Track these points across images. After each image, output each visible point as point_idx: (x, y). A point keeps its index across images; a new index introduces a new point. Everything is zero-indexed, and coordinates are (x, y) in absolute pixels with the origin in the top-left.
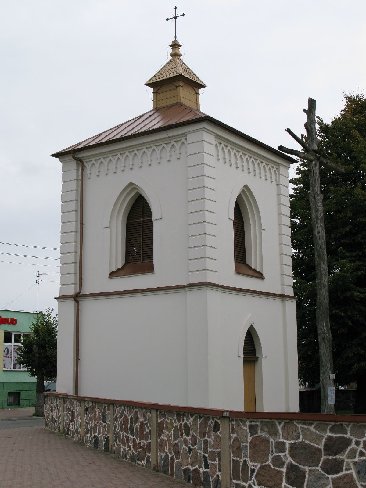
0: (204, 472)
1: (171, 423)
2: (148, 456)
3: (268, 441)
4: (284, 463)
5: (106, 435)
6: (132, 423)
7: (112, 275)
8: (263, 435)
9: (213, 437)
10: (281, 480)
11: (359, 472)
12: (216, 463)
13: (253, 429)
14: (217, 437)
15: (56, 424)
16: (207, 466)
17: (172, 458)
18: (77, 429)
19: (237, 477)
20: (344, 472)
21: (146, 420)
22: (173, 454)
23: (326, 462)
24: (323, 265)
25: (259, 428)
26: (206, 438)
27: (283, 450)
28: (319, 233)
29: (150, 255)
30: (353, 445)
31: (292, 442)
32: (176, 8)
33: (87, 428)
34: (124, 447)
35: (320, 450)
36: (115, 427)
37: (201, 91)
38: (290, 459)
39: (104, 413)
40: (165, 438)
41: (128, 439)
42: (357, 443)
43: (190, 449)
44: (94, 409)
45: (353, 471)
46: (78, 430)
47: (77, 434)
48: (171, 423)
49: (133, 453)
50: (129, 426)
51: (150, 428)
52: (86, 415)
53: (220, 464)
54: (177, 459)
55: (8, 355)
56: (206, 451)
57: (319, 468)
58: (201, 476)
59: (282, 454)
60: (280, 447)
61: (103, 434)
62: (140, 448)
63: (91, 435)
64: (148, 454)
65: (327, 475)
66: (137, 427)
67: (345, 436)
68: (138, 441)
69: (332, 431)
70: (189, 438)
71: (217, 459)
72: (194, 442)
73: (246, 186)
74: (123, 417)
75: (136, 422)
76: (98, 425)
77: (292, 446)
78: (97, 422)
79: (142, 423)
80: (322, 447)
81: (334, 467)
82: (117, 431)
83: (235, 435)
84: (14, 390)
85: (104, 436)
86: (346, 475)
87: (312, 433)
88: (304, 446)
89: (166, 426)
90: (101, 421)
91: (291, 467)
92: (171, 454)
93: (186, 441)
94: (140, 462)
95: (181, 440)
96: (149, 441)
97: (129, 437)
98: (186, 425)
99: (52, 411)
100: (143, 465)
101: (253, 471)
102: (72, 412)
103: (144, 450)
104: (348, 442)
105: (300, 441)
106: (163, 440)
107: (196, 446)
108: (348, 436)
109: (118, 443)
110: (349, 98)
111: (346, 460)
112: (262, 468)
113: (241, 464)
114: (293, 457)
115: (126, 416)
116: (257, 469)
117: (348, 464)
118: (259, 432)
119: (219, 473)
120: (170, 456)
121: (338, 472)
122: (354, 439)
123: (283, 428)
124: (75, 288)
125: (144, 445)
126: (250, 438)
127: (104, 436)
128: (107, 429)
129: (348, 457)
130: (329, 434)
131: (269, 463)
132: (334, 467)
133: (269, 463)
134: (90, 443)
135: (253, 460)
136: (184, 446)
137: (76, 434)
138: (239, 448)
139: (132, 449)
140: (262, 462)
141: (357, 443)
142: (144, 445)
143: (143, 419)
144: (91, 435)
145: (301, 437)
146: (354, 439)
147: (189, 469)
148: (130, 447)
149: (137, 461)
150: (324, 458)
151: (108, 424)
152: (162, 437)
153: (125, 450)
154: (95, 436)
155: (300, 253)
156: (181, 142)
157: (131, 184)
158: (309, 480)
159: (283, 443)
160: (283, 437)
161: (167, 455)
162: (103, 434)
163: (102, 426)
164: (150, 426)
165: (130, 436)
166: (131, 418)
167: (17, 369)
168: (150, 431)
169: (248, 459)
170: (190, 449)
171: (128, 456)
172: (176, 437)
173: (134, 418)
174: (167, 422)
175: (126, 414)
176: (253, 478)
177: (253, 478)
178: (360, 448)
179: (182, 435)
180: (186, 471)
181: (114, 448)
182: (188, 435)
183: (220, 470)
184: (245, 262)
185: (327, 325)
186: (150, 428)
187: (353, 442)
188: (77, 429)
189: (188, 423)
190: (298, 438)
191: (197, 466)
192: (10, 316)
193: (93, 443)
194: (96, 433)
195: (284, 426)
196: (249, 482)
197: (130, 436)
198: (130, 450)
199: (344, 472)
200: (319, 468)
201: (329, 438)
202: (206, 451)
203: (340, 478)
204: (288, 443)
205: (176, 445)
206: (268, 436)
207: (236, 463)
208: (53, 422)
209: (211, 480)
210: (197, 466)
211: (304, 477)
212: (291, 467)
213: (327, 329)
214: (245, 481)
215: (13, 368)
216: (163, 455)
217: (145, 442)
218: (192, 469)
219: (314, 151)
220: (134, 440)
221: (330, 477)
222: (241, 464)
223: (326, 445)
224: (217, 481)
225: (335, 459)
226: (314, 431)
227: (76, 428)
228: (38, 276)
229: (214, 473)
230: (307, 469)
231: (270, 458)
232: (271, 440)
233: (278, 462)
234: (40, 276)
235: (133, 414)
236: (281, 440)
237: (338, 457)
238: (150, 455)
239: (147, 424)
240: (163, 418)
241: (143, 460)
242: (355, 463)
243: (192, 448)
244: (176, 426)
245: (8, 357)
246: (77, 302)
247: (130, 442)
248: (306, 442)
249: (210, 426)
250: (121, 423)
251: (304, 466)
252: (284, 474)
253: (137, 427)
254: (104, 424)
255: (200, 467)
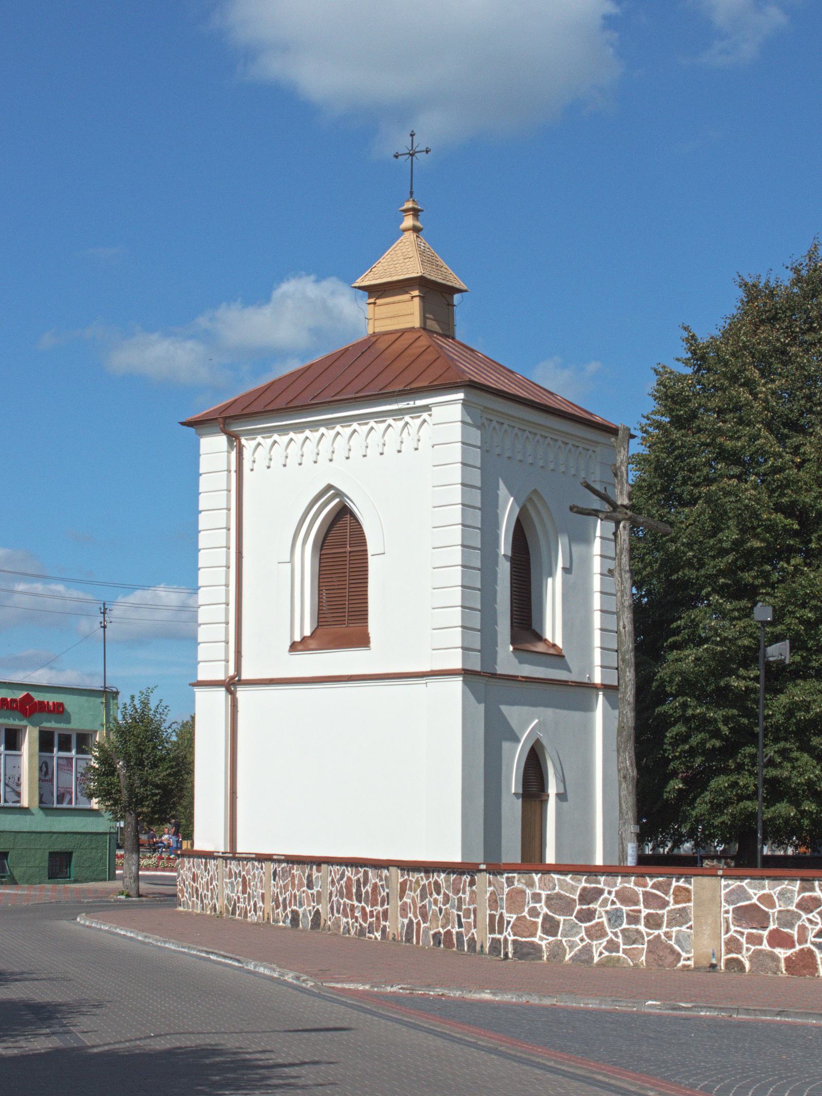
0: (457, 933)
1: (417, 882)
2: (385, 926)
3: (524, 892)
4: (539, 914)
5: (314, 907)
6: (359, 886)
7: (294, 647)
8: (520, 886)
9: (468, 893)
10: (536, 929)
11: (609, 920)
12: (471, 920)
13: (510, 881)
14: (472, 892)
15: (205, 901)
16: (460, 925)
17: (418, 924)
18: (255, 904)
19: (492, 931)
20: (596, 920)
21: (381, 880)
22: (420, 918)
23: (580, 912)
24: (628, 674)
25: (516, 879)
26: (461, 894)
27: (539, 901)
28: (624, 628)
29: (361, 614)
30: (606, 895)
31: (549, 892)
32: (412, 135)
33: (276, 900)
34: (345, 920)
35: (574, 900)
36: (331, 894)
37: (457, 297)
38: (545, 910)
39: (310, 876)
40: (409, 901)
41: (353, 908)
42: (610, 893)
43: (441, 910)
44: (290, 871)
45: (604, 920)
46: (258, 906)
47: (255, 911)
48: (417, 882)
49: (361, 925)
50: (354, 890)
51: (387, 890)
52: (273, 882)
53: (475, 921)
54: (424, 922)
55: (47, 778)
56: (459, 909)
57: (573, 918)
58: (454, 937)
59: (538, 905)
60: (536, 897)
61: (309, 905)
62: (372, 916)
63: (285, 908)
64: (384, 923)
65: (580, 924)
66: (367, 892)
67: (599, 886)
68: (368, 909)
69: (586, 881)
70: (440, 898)
71: (472, 916)
72: (447, 899)
73: (535, 491)
74: (345, 879)
75: (365, 886)
76: (298, 894)
77: (549, 898)
78: (296, 890)
79: (375, 885)
80: (576, 897)
81: (587, 916)
82: (334, 898)
83: (492, 888)
84: (58, 848)
85: (311, 908)
86: (598, 923)
87: (568, 884)
88: (559, 896)
89: (411, 886)
90: (305, 888)
91: (546, 918)
92: (416, 917)
93: (436, 901)
94: (371, 935)
95: (429, 901)
96: (386, 906)
97: (353, 905)
98: (436, 883)
99: (194, 880)
100: (376, 938)
101: (509, 922)
102: (244, 878)
103: (378, 918)
104: (601, 892)
105: (556, 891)
106: (406, 903)
107: (448, 906)
108: (601, 886)
109: (336, 915)
110: (752, 292)
111: (599, 909)
112: (518, 919)
113: (497, 917)
114: (548, 907)
115: (349, 879)
116: (512, 921)
117: (600, 913)
118: (516, 883)
119: (473, 931)
120: (415, 921)
121: (590, 920)
122: (607, 889)
123: (540, 879)
124: (227, 669)
125: (379, 912)
126: (506, 890)
127: (311, 908)
128: (318, 898)
129: (601, 906)
130: (584, 884)
131: (525, 914)
132: (587, 916)
133: (525, 914)
134: (284, 922)
135: (510, 911)
136: (433, 907)
137: (253, 912)
138: (496, 901)
139: (360, 920)
140: (518, 913)
141: (610, 893)
142: (379, 912)
143: (377, 880)
144: (285, 908)
145: (557, 888)
146: (607, 889)
147: (439, 933)
148: (356, 918)
149: (368, 935)
150: (578, 907)
151: (318, 892)
152: (405, 899)
153: (347, 923)
154: (293, 911)
155: (643, 596)
156: (421, 420)
157: (330, 487)
158: (564, 929)
159: (539, 894)
160: (540, 888)
161: (411, 921)
162: (309, 905)
163: (307, 895)
164: (388, 887)
165: (356, 903)
166: (358, 880)
167: (65, 805)
168: (388, 894)
169: (504, 911)
170: (441, 910)
171: (352, 932)
172: (423, 897)
173: (362, 880)
174: (411, 881)
175: (349, 875)
176: (509, 929)
177: (509, 929)
178: (612, 897)
179: (431, 894)
180: (436, 936)
181: (329, 923)
182: (438, 894)
183: (475, 927)
184: (530, 625)
185: (630, 758)
186: (387, 890)
187: (606, 892)
188: (255, 904)
189: (439, 880)
190: (554, 889)
191: (449, 928)
192: (50, 698)
193: (288, 921)
194: (295, 905)
195: (541, 878)
196: (505, 934)
197: (356, 903)
198: (356, 921)
199: (596, 920)
200: (573, 918)
201: (584, 889)
202: (459, 909)
203: (592, 926)
204: (544, 894)
205: (424, 906)
206: (524, 887)
207: (492, 917)
208: (197, 898)
209: (465, 939)
210: (449, 928)
211: (559, 926)
212: (546, 918)
213: (631, 764)
214: (501, 932)
215: (58, 803)
216: (406, 921)
217: (379, 908)
218: (442, 931)
219: (623, 506)
220: (363, 909)
221: (584, 925)
222: (497, 917)
223: (581, 895)
224: (472, 941)
225: (589, 909)
226: (570, 882)
227: (252, 903)
228: (104, 613)
229: (468, 932)
230: (562, 918)
231: (526, 909)
232: (528, 891)
233: (534, 912)
234: (108, 611)
235: (361, 874)
236: (538, 891)
237: (591, 906)
238: (387, 924)
239: (382, 886)
240: (406, 877)
241: (377, 931)
242: (607, 912)
243: (444, 907)
244: (424, 886)
245: (47, 781)
246: (232, 693)
247: (357, 911)
248: (562, 892)
249: (465, 881)
250: (341, 887)
251: (559, 915)
252: (540, 925)
253: (367, 892)
254: (310, 891)
255: (453, 928)
